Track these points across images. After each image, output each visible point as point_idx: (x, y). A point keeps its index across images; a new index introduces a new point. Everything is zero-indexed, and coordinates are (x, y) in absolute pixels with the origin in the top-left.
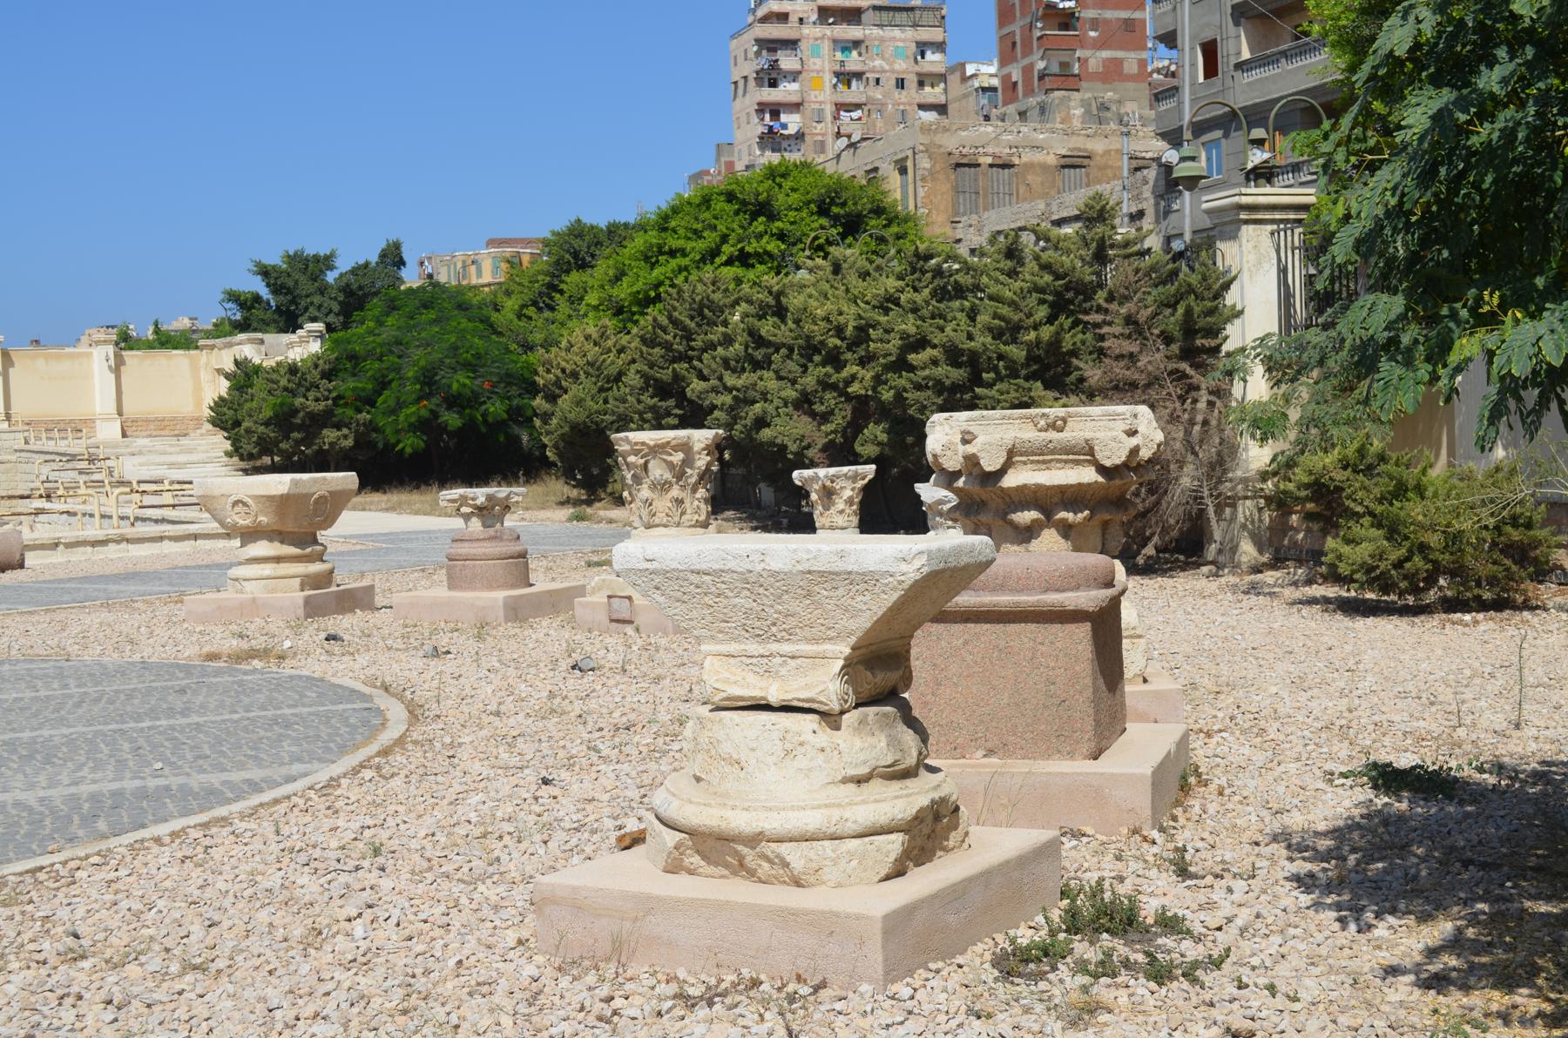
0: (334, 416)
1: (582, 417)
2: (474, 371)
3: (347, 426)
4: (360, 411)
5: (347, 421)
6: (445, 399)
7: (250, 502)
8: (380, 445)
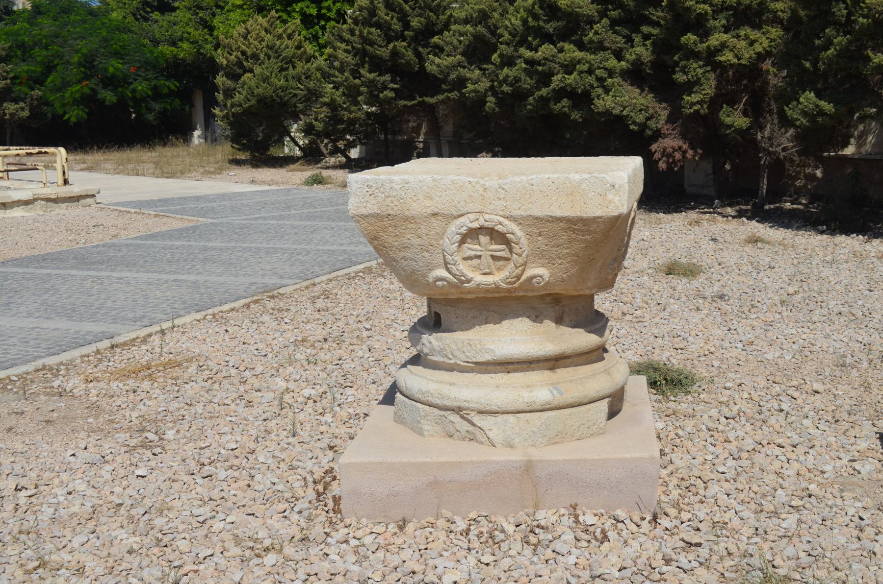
0: (13, 92)
1: (270, 91)
2: (122, 59)
3: (22, 100)
4: (33, 89)
5: (22, 96)
6: (102, 80)
7: (516, 231)
8: (49, 115)
